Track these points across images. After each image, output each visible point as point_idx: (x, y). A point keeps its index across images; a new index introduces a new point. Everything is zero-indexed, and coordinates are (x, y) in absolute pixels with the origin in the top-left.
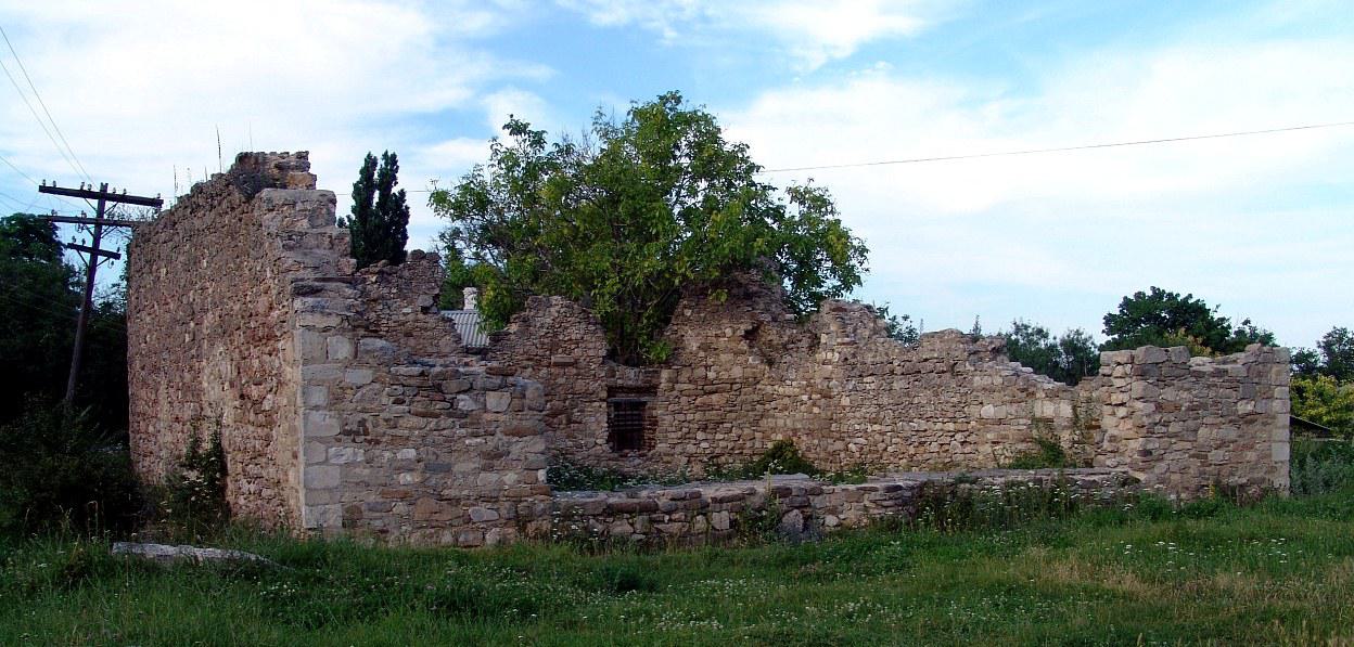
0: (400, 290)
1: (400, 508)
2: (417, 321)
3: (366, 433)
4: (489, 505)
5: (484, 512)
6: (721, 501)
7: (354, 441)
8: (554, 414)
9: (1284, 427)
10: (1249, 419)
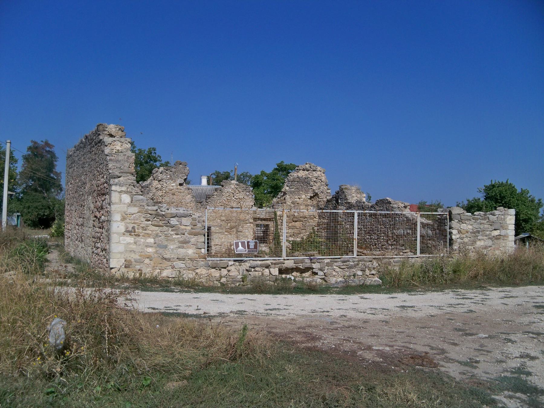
0: (171, 176)
1: (147, 261)
2: (177, 189)
3: (135, 232)
4: (182, 262)
5: (180, 264)
6: (275, 264)
7: (130, 235)
8: (231, 228)
9: (512, 241)
10: (498, 237)
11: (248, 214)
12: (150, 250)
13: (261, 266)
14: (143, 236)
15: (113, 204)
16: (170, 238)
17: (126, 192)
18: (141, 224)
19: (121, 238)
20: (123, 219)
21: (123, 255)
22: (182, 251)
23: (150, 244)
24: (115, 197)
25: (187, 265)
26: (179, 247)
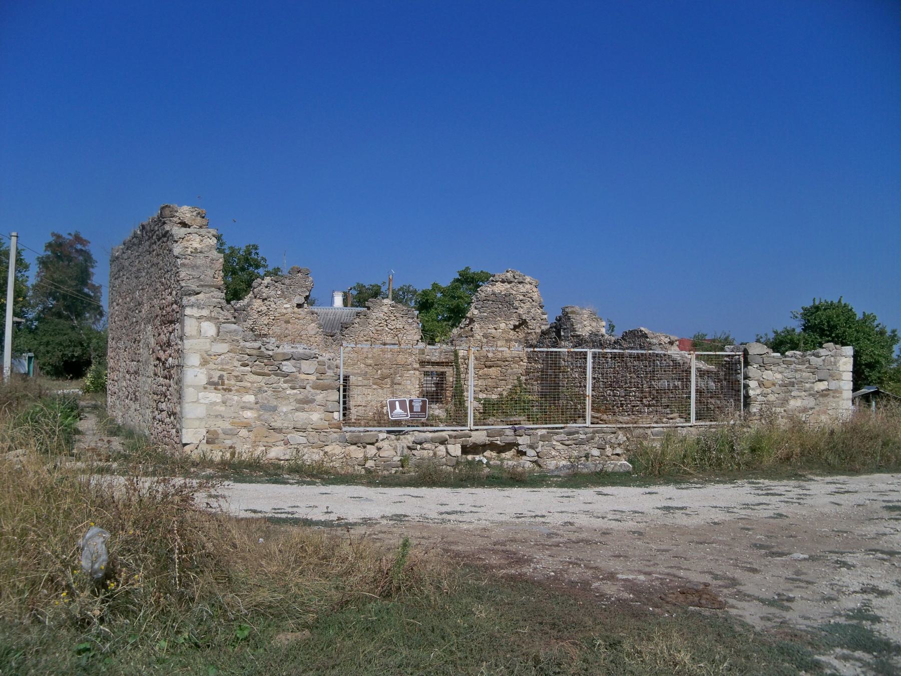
0: (283, 292)
1: (243, 432)
2: (294, 313)
3: (223, 384)
4: (301, 434)
5: (298, 438)
6: (455, 437)
7: (215, 389)
8: (383, 378)
9: (847, 399)
10: (825, 393)
11: (411, 354)
12: (248, 414)
13: (433, 441)
14: (237, 391)
15: (188, 338)
16: (281, 395)
17: (209, 319)
18: (233, 370)
19: (201, 395)
20: (204, 363)
21: (204, 423)
22: (301, 416)
23: (248, 405)
24: (190, 326)
25: (310, 438)
26: (297, 410)
